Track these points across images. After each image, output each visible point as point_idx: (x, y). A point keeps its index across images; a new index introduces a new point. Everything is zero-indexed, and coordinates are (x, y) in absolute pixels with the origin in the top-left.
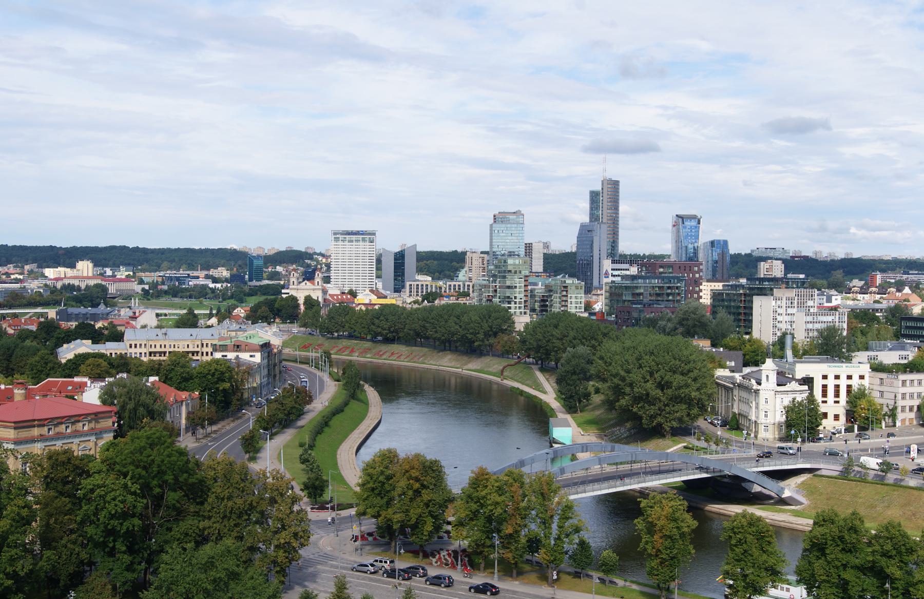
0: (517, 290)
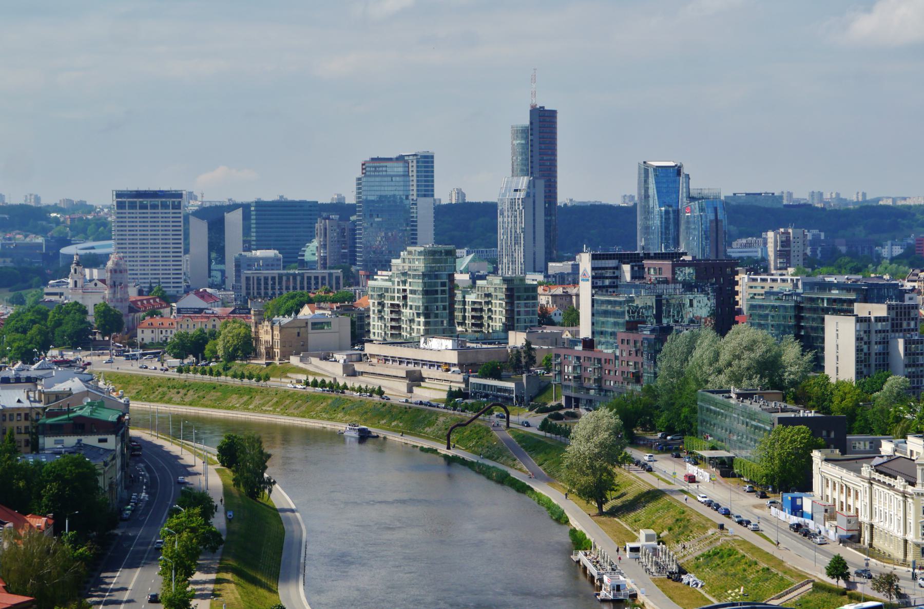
0: (439, 296)
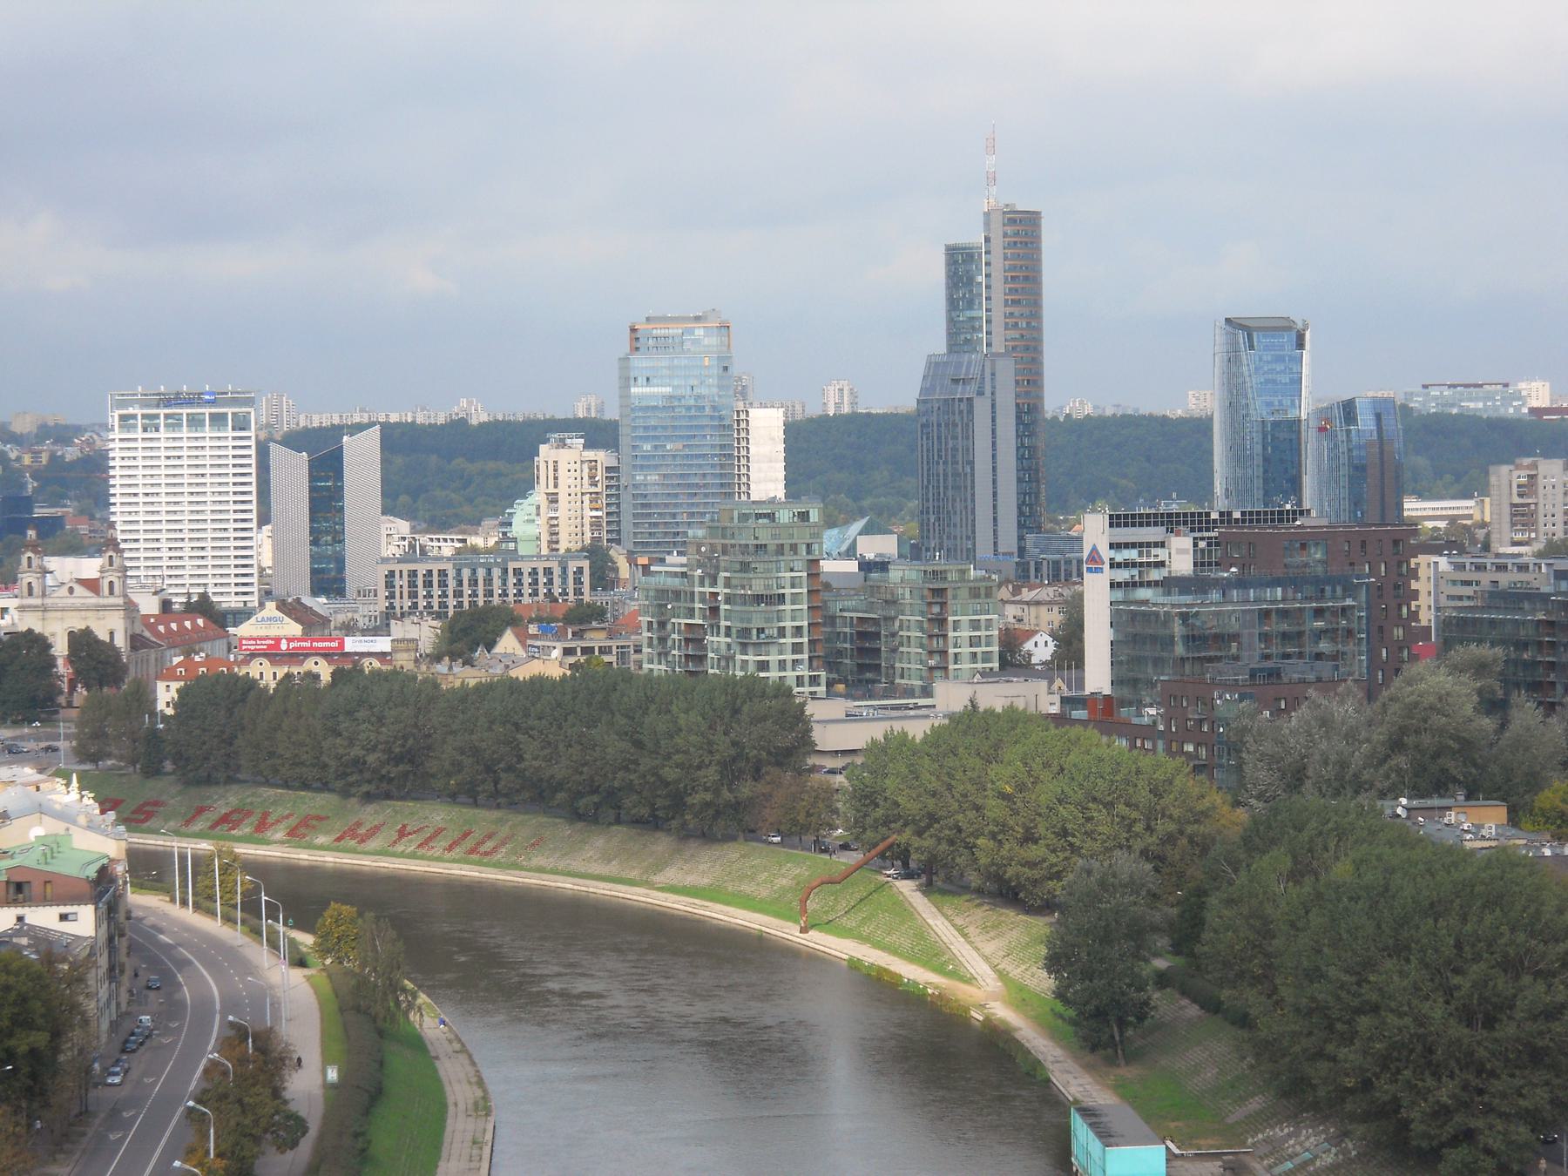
0: (788, 607)
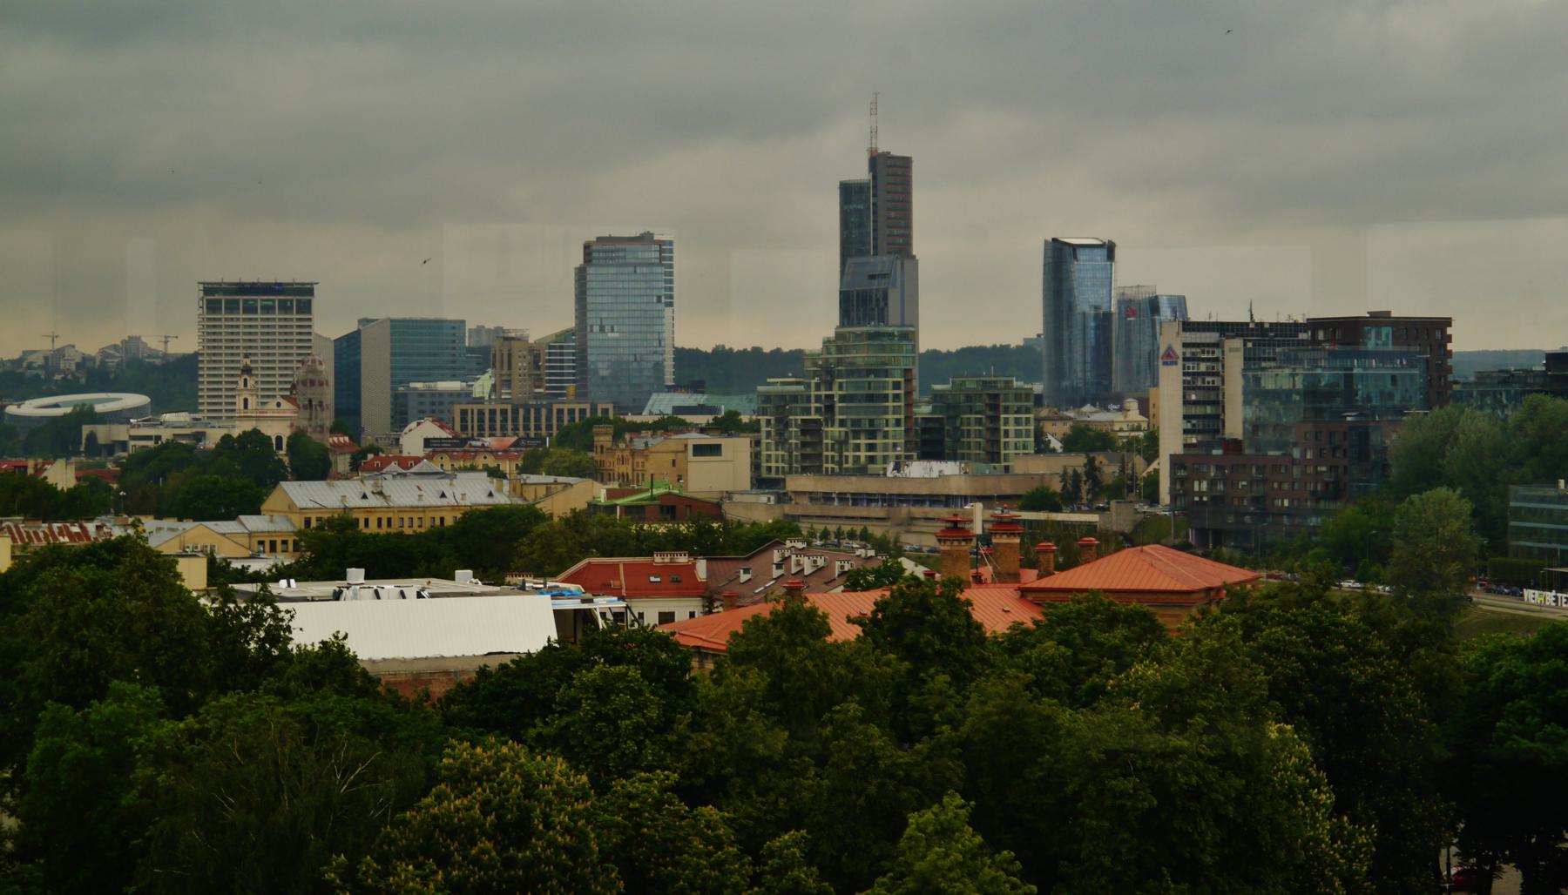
0: (890, 404)
